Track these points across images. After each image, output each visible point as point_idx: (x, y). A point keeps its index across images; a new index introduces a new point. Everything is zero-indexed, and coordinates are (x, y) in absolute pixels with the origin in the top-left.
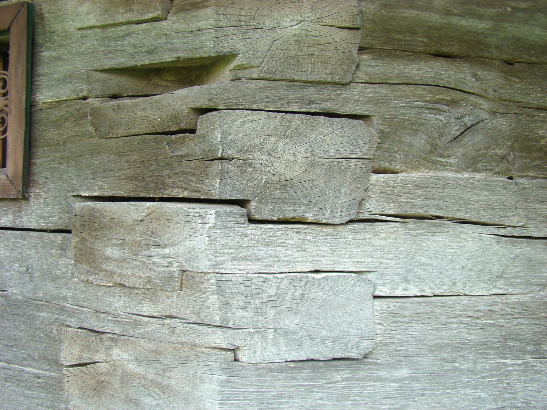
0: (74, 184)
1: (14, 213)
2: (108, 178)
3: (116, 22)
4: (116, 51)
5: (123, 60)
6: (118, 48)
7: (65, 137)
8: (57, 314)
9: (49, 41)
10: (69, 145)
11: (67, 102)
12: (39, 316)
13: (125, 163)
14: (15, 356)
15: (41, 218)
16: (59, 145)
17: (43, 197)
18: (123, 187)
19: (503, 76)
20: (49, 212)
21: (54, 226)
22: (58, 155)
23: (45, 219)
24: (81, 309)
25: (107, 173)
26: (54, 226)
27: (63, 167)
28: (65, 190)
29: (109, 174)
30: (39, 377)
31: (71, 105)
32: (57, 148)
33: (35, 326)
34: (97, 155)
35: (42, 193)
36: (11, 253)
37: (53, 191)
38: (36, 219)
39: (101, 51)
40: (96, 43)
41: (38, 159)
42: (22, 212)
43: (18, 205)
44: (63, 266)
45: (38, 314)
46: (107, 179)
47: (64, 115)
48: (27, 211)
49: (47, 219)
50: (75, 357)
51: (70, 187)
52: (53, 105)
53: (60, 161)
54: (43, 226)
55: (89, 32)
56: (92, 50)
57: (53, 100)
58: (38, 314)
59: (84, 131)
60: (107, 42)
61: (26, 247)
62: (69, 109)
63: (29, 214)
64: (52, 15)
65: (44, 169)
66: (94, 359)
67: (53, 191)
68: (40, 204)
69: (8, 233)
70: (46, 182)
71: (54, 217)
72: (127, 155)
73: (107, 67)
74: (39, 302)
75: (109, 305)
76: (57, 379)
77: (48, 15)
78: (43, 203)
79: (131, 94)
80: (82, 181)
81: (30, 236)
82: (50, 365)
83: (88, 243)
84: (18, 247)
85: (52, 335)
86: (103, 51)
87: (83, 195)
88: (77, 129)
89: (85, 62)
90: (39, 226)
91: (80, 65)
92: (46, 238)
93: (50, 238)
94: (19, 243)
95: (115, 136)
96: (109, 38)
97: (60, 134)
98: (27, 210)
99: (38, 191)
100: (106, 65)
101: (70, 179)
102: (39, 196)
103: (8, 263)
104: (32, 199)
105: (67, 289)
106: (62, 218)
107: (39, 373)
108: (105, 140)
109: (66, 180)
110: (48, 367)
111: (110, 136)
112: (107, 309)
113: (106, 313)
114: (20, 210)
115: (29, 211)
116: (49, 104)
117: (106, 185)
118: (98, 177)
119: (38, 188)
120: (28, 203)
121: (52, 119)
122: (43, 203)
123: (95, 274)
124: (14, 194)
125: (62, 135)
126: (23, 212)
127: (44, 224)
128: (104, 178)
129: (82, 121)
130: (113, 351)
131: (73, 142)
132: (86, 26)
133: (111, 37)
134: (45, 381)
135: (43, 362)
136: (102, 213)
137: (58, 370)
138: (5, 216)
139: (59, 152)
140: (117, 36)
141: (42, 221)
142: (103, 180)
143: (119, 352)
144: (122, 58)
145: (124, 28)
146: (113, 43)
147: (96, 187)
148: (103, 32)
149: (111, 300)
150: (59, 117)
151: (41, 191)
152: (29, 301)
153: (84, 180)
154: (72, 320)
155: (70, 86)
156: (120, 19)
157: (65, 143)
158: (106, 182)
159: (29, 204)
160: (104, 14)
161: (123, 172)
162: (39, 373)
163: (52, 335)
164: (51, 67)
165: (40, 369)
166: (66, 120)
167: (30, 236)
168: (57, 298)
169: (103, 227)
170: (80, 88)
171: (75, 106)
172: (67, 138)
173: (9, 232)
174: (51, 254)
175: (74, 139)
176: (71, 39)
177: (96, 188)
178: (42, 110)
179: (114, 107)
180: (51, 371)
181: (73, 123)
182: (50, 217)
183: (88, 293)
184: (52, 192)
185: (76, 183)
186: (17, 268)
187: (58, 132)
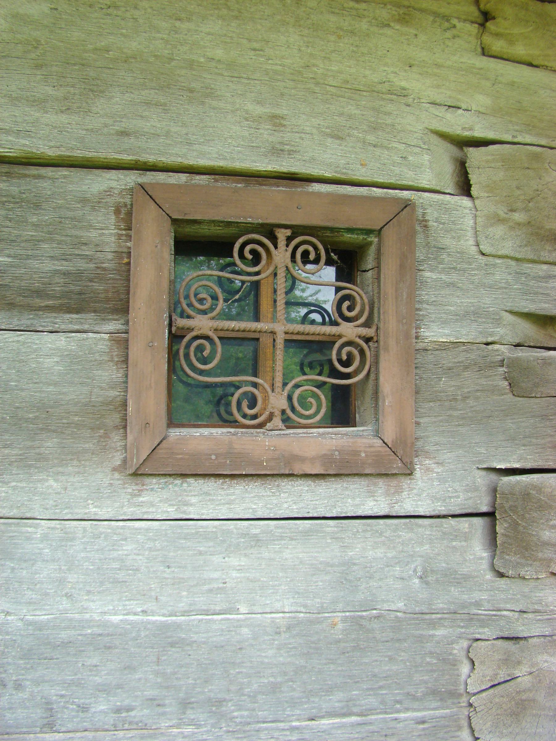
0: (482, 453)
1: (387, 494)
2: (529, 446)
3: (542, 259)
4: (536, 293)
5: (547, 305)
6: (540, 290)
7: (466, 390)
8: (462, 627)
9: (435, 259)
10: (471, 402)
11: (466, 346)
12: (433, 636)
13: (550, 428)
14: (383, 702)
15: (438, 500)
16: (455, 400)
17: (435, 470)
18: (551, 457)
19: (306, 300)
20: (449, 491)
21: (460, 509)
22: (455, 413)
23: (444, 500)
24: (499, 613)
25: (527, 439)
26: (459, 509)
27: (463, 430)
28: (470, 461)
29: (531, 442)
30: (423, 722)
31: (473, 350)
32: (454, 405)
33: (424, 651)
34: (512, 417)
35: (433, 465)
36: (385, 553)
37: (452, 462)
38: (429, 502)
39: (517, 289)
40: (509, 278)
41: (422, 417)
42: (402, 492)
43: (394, 482)
44: (472, 562)
45: (431, 632)
46: (528, 447)
47: (462, 362)
48: (412, 490)
49: (447, 501)
50: (488, 678)
51: (477, 457)
52: (444, 347)
53: (458, 421)
54: (441, 509)
55: (498, 261)
56: (503, 285)
57: (448, 341)
58: (431, 632)
59: (492, 384)
60: (523, 279)
61: (413, 542)
62: (469, 355)
63: (415, 495)
64: (441, 226)
65: (433, 433)
66: (514, 674)
67: (452, 462)
68: (431, 479)
69: (329, 526)
70: (438, 450)
71: (458, 497)
72: (551, 419)
73: (526, 310)
74: (434, 616)
75: (540, 602)
76: (454, 716)
77: (435, 224)
78: (437, 479)
79: (532, 344)
80: (493, 449)
81: (420, 526)
82: (441, 700)
83: (521, 528)
84: (399, 542)
85: (451, 657)
86: (520, 289)
87: (497, 467)
88: (483, 381)
89: (495, 298)
90: (434, 510)
91: (487, 301)
92: (445, 526)
93: (452, 526)
94: (399, 537)
95: (539, 396)
96: (527, 275)
97: (458, 386)
98: (411, 489)
99: (427, 462)
100: (525, 307)
101: (477, 446)
102: (428, 470)
103: (381, 568)
104: (418, 473)
105: (480, 591)
106: (471, 498)
107: (425, 715)
108: (521, 399)
109: (470, 447)
110: (439, 704)
111: (533, 395)
112: (536, 607)
113: (535, 612)
114: (399, 490)
115: (415, 491)
116: (437, 343)
117: (528, 455)
118: (517, 445)
119: (426, 457)
120: (410, 479)
121: (444, 364)
122: (437, 479)
123: (528, 565)
124: (398, 467)
125: (459, 388)
126: (405, 493)
127: (443, 508)
128: (524, 445)
129: (490, 373)
130: (540, 658)
131: (477, 398)
132: (500, 253)
133: (529, 275)
134: (434, 724)
135: (431, 699)
136: (539, 489)
137: (453, 703)
138: (371, 499)
139: (457, 410)
140: (536, 275)
141: (439, 504)
142: (523, 448)
143: (545, 657)
144: (545, 303)
145: (545, 267)
146: (532, 283)
147: (514, 457)
148: (517, 265)
149: (540, 595)
150: (455, 363)
151: (431, 462)
152: (418, 618)
153: (497, 448)
154: (486, 630)
155: (474, 325)
156: (547, 257)
157: (465, 398)
158: (528, 451)
159: (413, 481)
160: (526, 246)
161: (549, 439)
162: (424, 717)
163: (451, 657)
164: (440, 294)
165: (425, 709)
166: (466, 368)
167: (416, 525)
168: (464, 605)
169: (542, 507)
170: (491, 330)
171: (478, 352)
172: (469, 392)
173: (381, 521)
174: (454, 547)
175: (479, 394)
176: (470, 263)
177: (514, 459)
178: (426, 350)
179: (539, 361)
180: (443, 708)
181: (476, 373)
182: (450, 497)
183: (511, 592)
184: (449, 463)
185: (485, 452)
186: (396, 573)
187: (453, 383)
